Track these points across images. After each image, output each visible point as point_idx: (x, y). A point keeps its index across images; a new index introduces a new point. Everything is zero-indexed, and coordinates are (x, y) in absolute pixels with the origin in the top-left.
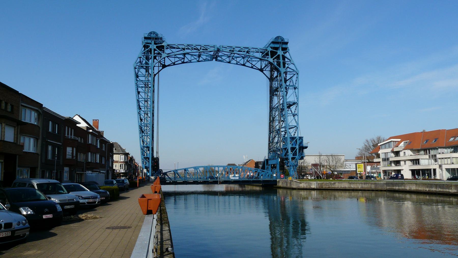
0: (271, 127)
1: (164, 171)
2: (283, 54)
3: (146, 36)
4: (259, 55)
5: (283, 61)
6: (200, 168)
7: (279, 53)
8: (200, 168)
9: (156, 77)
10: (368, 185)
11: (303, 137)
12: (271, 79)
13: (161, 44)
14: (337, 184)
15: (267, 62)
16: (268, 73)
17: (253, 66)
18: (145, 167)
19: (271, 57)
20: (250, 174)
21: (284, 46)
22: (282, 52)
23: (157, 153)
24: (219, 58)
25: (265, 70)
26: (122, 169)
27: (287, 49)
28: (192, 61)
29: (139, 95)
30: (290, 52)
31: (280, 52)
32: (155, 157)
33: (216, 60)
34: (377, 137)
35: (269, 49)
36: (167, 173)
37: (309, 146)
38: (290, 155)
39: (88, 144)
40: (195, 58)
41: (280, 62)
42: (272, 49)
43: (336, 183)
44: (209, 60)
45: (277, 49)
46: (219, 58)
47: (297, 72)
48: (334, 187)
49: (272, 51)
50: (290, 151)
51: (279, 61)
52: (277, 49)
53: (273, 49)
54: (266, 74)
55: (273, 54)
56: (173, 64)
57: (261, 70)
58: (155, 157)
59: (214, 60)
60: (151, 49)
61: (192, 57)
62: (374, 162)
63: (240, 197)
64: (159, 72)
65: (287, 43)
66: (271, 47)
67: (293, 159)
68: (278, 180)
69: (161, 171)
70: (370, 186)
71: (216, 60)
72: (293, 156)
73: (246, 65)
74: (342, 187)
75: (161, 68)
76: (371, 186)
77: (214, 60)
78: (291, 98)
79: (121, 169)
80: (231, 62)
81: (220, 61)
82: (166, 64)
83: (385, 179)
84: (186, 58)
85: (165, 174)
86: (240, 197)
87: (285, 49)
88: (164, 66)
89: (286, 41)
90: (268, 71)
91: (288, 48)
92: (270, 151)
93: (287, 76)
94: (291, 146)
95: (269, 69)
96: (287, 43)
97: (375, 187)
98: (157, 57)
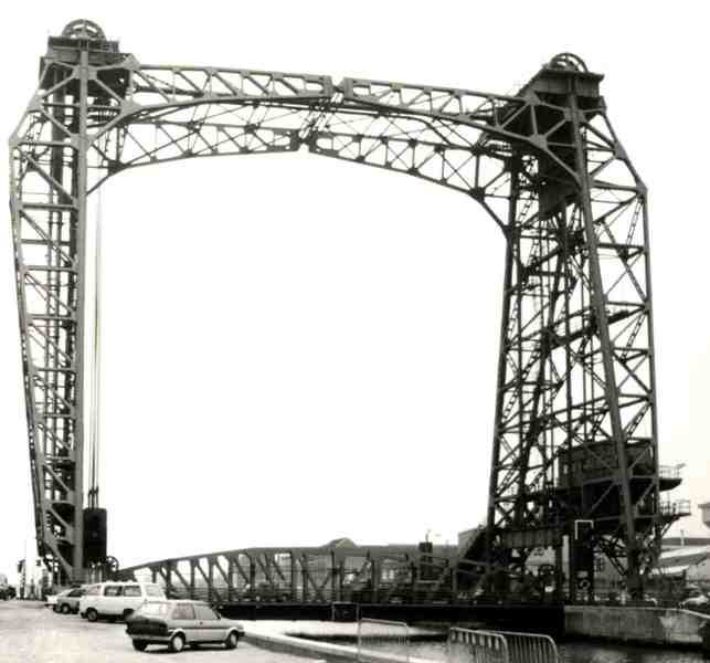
3: (58, 33)
4: (636, 293)
7: (567, 117)
12: (512, 232)
16: (502, 208)
17: (448, 172)
19: (541, 132)
21: (583, 91)
24: (323, 143)
28: (160, 155)
30: (609, 113)
31: (571, 113)
35: (532, 100)
37: (683, 474)
40: (614, 241)
41: (575, 150)
42: (541, 99)
44: (282, 149)
45: (559, 99)
46: (323, 143)
47: (641, 190)
49: (540, 106)
51: (571, 148)
52: (559, 99)
55: (547, 118)
56: (147, 159)
57: (478, 194)
59: (304, 148)
61: (221, 133)
62: (481, 132)
63: (524, 536)
65: (595, 80)
66: (539, 94)
72: (634, 474)
75: (105, 172)
77: (304, 148)
80: (367, 160)
82: (124, 160)
84: (500, 218)
86: (524, 536)
87: (593, 105)
88: (115, 167)
89: (593, 69)
93: (25, 383)
95: (506, 189)
96: (595, 80)
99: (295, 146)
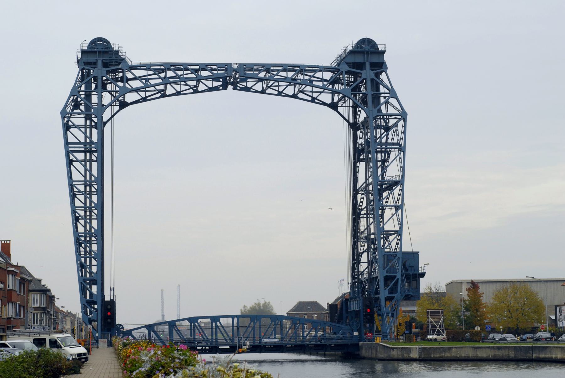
0: (381, 222)
1: (126, 328)
2: (373, 77)
5: (373, 93)
6: (221, 320)
7: (364, 76)
8: (221, 320)
9: (107, 129)
10: (503, 351)
11: (419, 252)
12: (354, 126)
13: (116, 65)
14: (454, 350)
15: (338, 96)
18: (89, 321)
20: (368, 331)
21: (375, 59)
22: (372, 72)
23: (112, 289)
25: (341, 106)
26: (37, 323)
27: (383, 67)
29: (72, 166)
30: (388, 72)
32: (107, 299)
33: (234, 89)
34: (267, 302)
36: (133, 332)
38: (384, 293)
39: (8, 290)
43: (452, 347)
48: (449, 355)
50: (382, 283)
53: (354, 68)
54: (342, 114)
57: (333, 106)
58: (107, 299)
59: (230, 87)
60: (97, 76)
64: (113, 116)
66: (348, 64)
67: (389, 299)
68: (360, 343)
69: (121, 328)
70: (507, 354)
71: (234, 89)
73: (300, 97)
74: (463, 355)
75: (117, 108)
76: (509, 352)
77: (230, 87)
78: (393, 172)
79: (34, 323)
81: (242, 89)
83: (3, 329)
85: (129, 332)
88: (124, 105)
90: (347, 108)
91: (384, 64)
92: (354, 281)
94: (385, 274)
97: (515, 355)
98: (108, 86)
99: (225, 87)
